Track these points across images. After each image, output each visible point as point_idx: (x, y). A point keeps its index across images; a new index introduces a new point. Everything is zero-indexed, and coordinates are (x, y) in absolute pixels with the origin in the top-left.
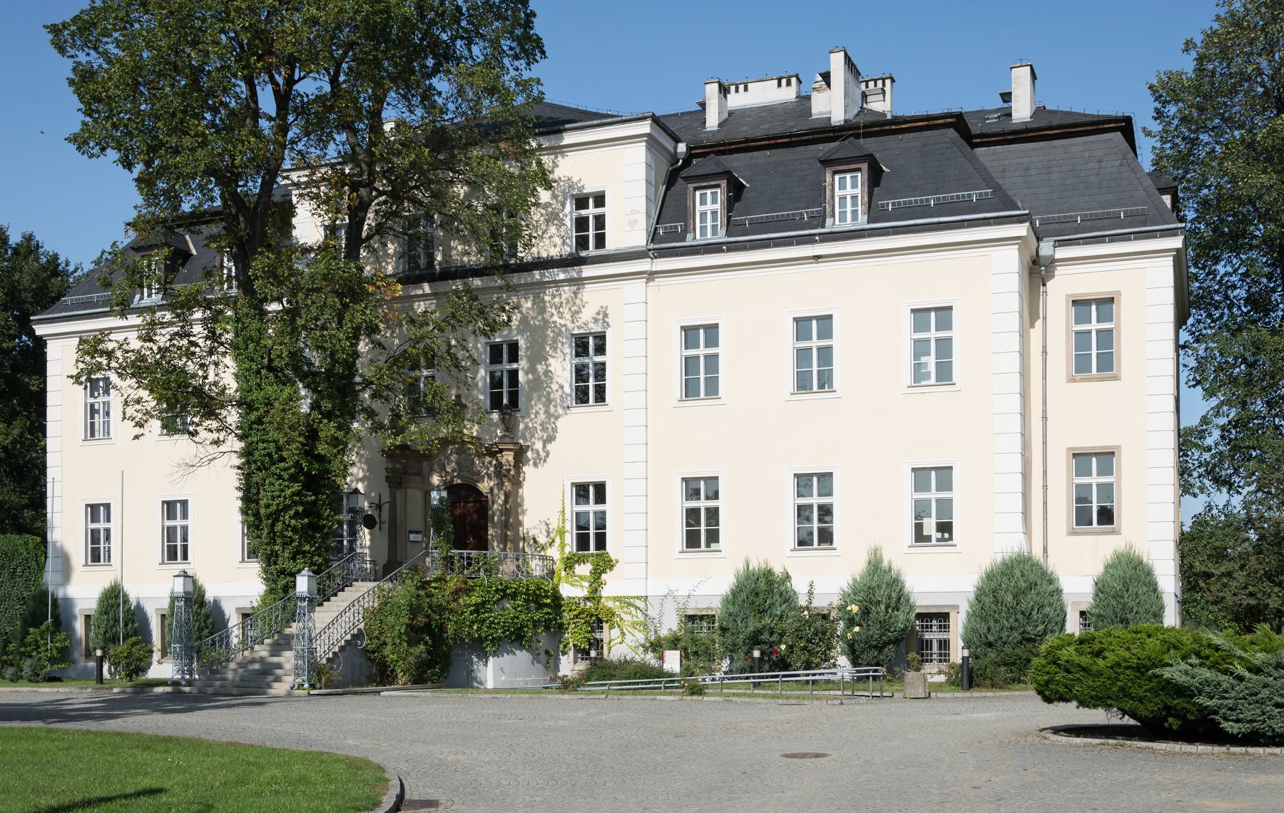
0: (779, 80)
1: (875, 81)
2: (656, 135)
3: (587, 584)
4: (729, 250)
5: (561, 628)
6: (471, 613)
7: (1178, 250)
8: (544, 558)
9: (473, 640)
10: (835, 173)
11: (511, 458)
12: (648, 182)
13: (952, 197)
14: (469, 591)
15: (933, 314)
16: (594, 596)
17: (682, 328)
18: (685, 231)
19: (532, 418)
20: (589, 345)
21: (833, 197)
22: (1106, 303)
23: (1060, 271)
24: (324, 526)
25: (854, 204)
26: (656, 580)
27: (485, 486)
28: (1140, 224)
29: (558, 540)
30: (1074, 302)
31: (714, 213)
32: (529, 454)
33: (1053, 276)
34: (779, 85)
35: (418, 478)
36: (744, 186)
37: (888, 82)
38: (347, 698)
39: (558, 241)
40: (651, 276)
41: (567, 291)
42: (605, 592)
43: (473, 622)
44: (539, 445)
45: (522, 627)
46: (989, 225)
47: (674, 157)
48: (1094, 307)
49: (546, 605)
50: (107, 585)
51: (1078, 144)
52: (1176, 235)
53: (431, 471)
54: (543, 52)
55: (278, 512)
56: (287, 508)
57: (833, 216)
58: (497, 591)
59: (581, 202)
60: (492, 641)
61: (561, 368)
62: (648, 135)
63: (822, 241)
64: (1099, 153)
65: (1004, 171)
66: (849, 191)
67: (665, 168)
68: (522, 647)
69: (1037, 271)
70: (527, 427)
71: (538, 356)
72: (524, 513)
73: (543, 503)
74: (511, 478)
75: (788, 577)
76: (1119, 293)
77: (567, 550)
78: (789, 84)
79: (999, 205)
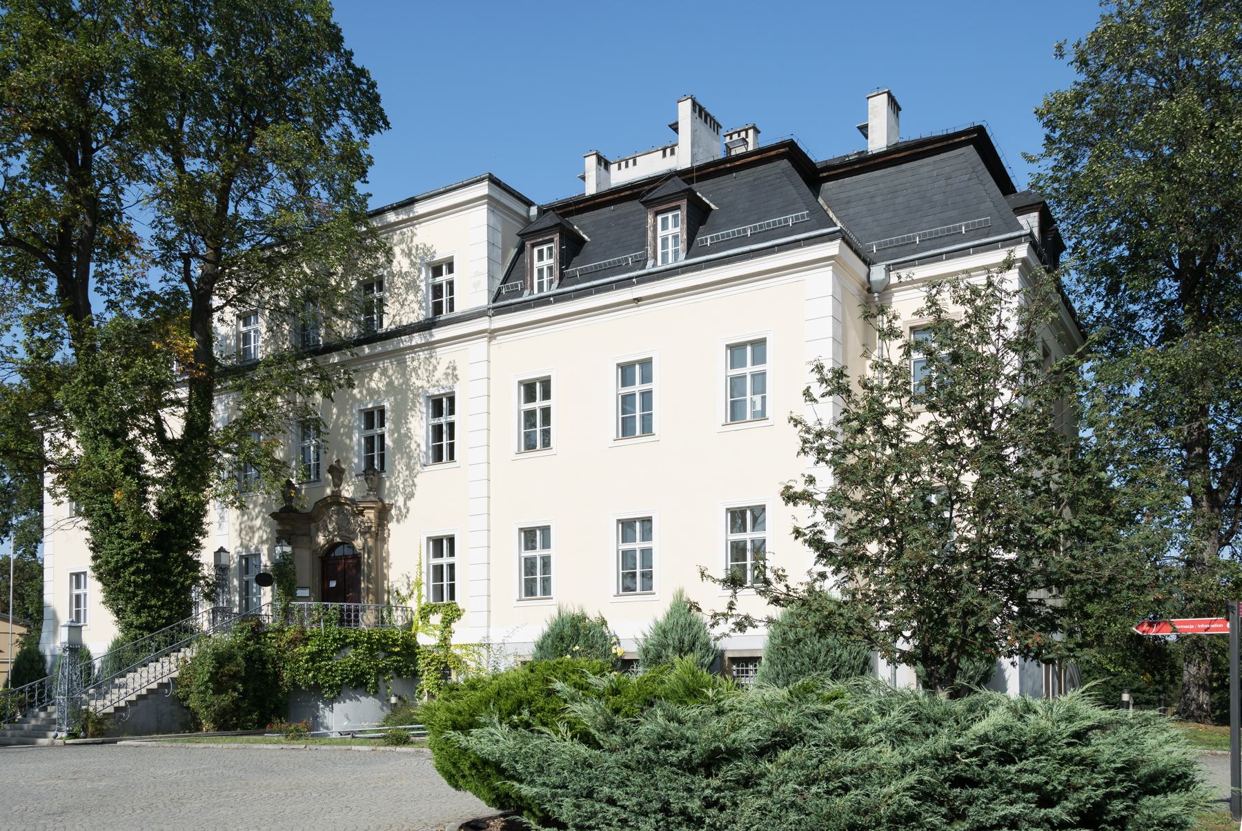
0: (664, 150)
1: (739, 133)
3: (438, 633)
4: (556, 301)
5: (415, 675)
6: (307, 662)
8: (404, 610)
9: (309, 686)
10: (657, 214)
12: (491, 244)
13: (769, 224)
14: (306, 641)
16: (445, 643)
18: (523, 289)
19: (396, 479)
20: (441, 405)
24: (176, 582)
25: (676, 244)
29: (416, 592)
31: (550, 268)
32: (393, 512)
34: (664, 155)
35: (306, 539)
36: (584, 241)
37: (751, 132)
39: (416, 306)
40: (492, 334)
42: (454, 640)
43: (308, 671)
44: (400, 502)
46: (800, 246)
47: (527, 220)
49: (397, 654)
51: (928, 164)
52: (1020, 243)
53: (318, 530)
56: (126, 565)
57: (656, 259)
58: (335, 640)
60: (330, 687)
61: (419, 426)
62: (488, 196)
63: (639, 283)
64: (947, 170)
68: (367, 694)
70: (391, 485)
72: (388, 567)
73: (404, 560)
74: (379, 533)
75: (604, 623)
77: (424, 600)
79: (816, 227)
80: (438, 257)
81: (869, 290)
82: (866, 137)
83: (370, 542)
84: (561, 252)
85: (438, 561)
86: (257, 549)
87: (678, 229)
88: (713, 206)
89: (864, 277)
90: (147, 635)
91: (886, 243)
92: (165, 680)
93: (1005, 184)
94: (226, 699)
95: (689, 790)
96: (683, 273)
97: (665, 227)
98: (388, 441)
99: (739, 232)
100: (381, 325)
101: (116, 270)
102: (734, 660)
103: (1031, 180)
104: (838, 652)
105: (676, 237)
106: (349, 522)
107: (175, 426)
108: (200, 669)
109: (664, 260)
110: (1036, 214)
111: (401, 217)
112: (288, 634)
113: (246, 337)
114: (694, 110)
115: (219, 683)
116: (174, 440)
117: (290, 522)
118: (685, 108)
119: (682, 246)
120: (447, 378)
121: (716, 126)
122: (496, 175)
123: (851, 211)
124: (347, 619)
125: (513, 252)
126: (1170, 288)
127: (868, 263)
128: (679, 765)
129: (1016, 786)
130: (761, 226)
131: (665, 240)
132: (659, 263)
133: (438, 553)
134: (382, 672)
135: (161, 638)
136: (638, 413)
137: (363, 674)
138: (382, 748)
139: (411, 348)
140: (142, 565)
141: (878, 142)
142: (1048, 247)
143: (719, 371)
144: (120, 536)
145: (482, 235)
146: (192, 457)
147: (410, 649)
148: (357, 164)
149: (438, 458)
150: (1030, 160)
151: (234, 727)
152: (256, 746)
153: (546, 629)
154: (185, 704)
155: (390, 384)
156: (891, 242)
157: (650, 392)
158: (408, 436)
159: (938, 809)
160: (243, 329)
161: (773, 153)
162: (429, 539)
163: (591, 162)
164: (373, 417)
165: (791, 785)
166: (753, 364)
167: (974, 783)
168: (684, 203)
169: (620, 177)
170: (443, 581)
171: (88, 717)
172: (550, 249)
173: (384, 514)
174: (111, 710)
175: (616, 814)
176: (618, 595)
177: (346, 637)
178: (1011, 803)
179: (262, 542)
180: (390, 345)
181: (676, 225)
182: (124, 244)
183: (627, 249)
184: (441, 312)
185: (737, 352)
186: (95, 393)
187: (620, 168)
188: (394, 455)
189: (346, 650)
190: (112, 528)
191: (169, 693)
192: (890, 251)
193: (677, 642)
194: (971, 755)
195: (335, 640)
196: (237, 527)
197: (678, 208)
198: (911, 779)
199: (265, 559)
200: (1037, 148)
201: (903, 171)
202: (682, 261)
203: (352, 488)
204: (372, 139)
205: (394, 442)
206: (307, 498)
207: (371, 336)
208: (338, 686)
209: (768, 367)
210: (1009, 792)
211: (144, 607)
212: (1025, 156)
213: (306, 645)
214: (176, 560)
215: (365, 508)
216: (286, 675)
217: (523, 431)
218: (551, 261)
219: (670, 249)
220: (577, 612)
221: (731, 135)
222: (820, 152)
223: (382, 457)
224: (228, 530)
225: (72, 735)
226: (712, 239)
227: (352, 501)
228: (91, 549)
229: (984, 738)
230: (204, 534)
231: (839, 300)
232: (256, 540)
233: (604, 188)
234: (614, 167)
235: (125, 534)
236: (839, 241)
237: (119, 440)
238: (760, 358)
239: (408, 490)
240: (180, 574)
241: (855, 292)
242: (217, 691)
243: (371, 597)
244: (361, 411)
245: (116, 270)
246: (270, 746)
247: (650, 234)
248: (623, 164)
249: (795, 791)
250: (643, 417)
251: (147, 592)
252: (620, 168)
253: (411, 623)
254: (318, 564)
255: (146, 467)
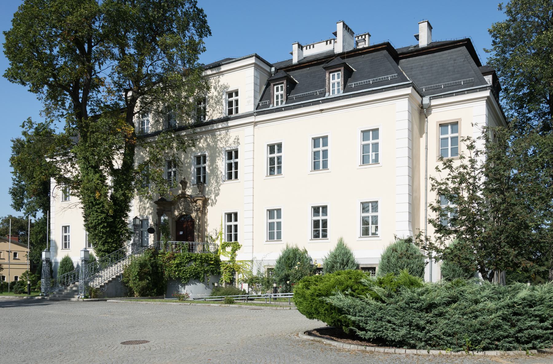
0: (327, 42)
1: (362, 36)
2: (258, 63)
3: (230, 255)
4: (285, 110)
5: (219, 274)
6: (175, 267)
7: (488, 97)
8: (214, 245)
9: (176, 278)
10: (330, 73)
11: (201, 203)
12: (255, 84)
13: (380, 79)
14: (174, 258)
15: (371, 132)
16: (233, 259)
17: (268, 145)
18: (270, 104)
20: (232, 154)
21: (329, 83)
22: (455, 125)
23: (434, 111)
24: (118, 232)
25: (338, 86)
26: (257, 253)
27: (194, 215)
28: (472, 86)
29: (220, 237)
30: (440, 125)
32: (209, 201)
33: (431, 114)
34: (327, 44)
36: (296, 83)
37: (367, 36)
38: (99, 302)
40: (256, 123)
41: (223, 132)
42: (237, 259)
43: (176, 271)
44: (213, 197)
45: (199, 273)
46: (394, 89)
47: (270, 74)
48: (449, 127)
49: (212, 264)
50: (64, 257)
51: (446, 54)
52: (487, 90)
53: (175, 209)
54: (210, 33)
55: (95, 226)
56: (99, 224)
57: (329, 92)
58: (187, 258)
59: (230, 95)
60: (185, 279)
61: (222, 164)
63: (323, 103)
64: (454, 56)
65: (412, 69)
66: (336, 80)
67: (266, 78)
68: (200, 282)
69: (423, 112)
70: (209, 190)
71: (213, 161)
72: (207, 226)
73: (214, 223)
74: (203, 211)
75: (306, 251)
76: (460, 119)
77: (223, 241)
78: (330, 43)
79: (399, 81)
80: (230, 89)
81: (422, 108)
82: (418, 40)
83: (200, 214)
84: (287, 88)
85: (230, 224)
86: (147, 216)
87: (339, 80)
88: (354, 70)
89: (420, 102)
90: (107, 255)
91: (429, 88)
92: (118, 274)
93: (478, 63)
94: (144, 283)
95: (420, 317)
96: (342, 99)
97: (333, 79)
98: (207, 170)
99: (367, 82)
100: (205, 119)
101: (95, 96)
102: (364, 269)
103: (488, 61)
104: (412, 265)
105: (338, 83)
106: (189, 206)
107: (118, 163)
108: (133, 270)
109: (333, 93)
110: (491, 76)
111: (215, 72)
112: (167, 255)
113: (143, 123)
114: (344, 27)
115: (141, 276)
116: (118, 170)
117: (163, 206)
118: (340, 26)
119: (341, 87)
120: (234, 144)
121: (352, 33)
122: (258, 54)
123: (413, 73)
124: (191, 249)
125: (264, 87)
126: (545, 107)
127: (422, 96)
128: (417, 309)
129: (533, 315)
130: (376, 80)
131: (333, 84)
132: (331, 94)
133: (230, 220)
134: (206, 272)
135: (113, 256)
136: (321, 160)
137: (199, 273)
138: (224, 305)
139: (219, 129)
140: (105, 224)
141: (423, 43)
142: (496, 89)
143: (358, 142)
144: (97, 212)
145: (251, 80)
146: (124, 177)
147: (217, 262)
148: (195, 49)
149: (230, 177)
150: (487, 51)
151: (147, 295)
152: (168, 303)
153: (281, 254)
154: (126, 285)
155: (208, 145)
156: (431, 87)
157: (327, 150)
158: (217, 168)
159: (507, 323)
160: (141, 120)
161: (380, 47)
162: (225, 213)
163: (296, 47)
164: (201, 159)
165: (457, 316)
166: (373, 139)
167: (520, 315)
168: (342, 69)
169: (308, 53)
170: (232, 233)
171: (91, 290)
172: (282, 87)
173: (205, 202)
174: (99, 287)
175: (391, 326)
176: (312, 240)
177: (192, 257)
178: (531, 321)
179: (150, 214)
180: (210, 127)
181: (338, 78)
182: (98, 83)
183: (316, 88)
184: (232, 113)
185: (365, 134)
186: (93, 150)
187: (307, 49)
188: (210, 176)
189: (191, 262)
190: (94, 208)
191: (121, 280)
192: (430, 91)
193: (341, 261)
194: (519, 305)
195: (187, 258)
196: (138, 207)
197: (340, 70)
198: (500, 313)
199: (151, 222)
200: (490, 47)
201: (435, 56)
202: (341, 94)
203: (191, 190)
204: (204, 39)
205: (210, 170)
206: (170, 194)
207: (200, 124)
208: (188, 278)
209: (380, 141)
210: (530, 318)
211: (106, 242)
212: (484, 50)
213: (175, 260)
214: (118, 222)
215: (197, 200)
216: (166, 273)
217: (269, 166)
218: (282, 92)
219: (336, 88)
220: (294, 247)
221: (358, 37)
222: (397, 45)
223: (204, 178)
224: (138, 209)
225: (86, 297)
226: (355, 84)
227: (191, 196)
228: (84, 217)
229: (524, 299)
230: (130, 211)
231: (410, 113)
232: (146, 213)
233: (301, 58)
234: (304, 48)
235: (99, 211)
236: (411, 88)
237: (97, 169)
238: (376, 136)
239: (217, 192)
240: (120, 228)
241: (416, 109)
242: (141, 279)
243: (200, 239)
244: (195, 156)
245: (95, 96)
246: (175, 303)
247: (327, 81)
248: (308, 47)
249: (459, 317)
250: (323, 161)
251: (107, 236)
252: (307, 49)
253: (218, 250)
254: (174, 224)
255: (107, 181)
